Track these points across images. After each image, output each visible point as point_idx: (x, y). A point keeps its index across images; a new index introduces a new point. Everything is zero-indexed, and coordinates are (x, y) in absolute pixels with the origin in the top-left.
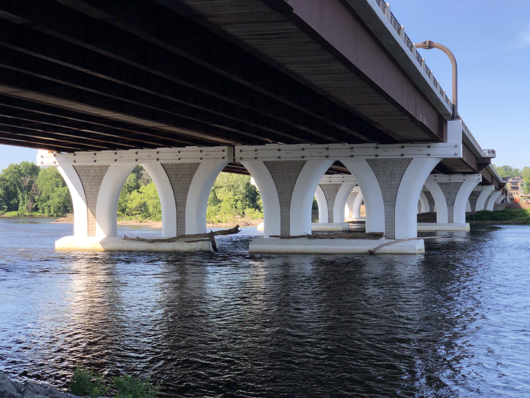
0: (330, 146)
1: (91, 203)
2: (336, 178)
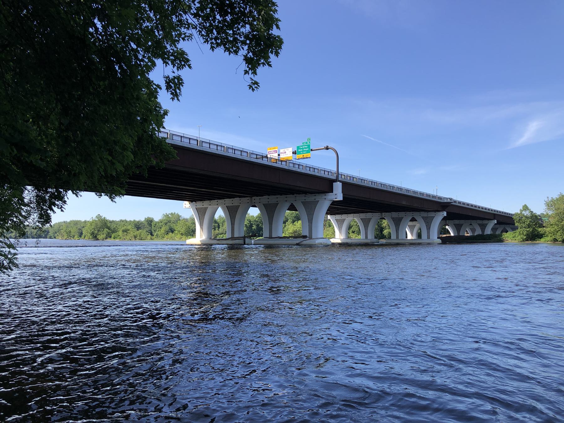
0: (287, 196)
1: (201, 225)
2: (414, 223)
